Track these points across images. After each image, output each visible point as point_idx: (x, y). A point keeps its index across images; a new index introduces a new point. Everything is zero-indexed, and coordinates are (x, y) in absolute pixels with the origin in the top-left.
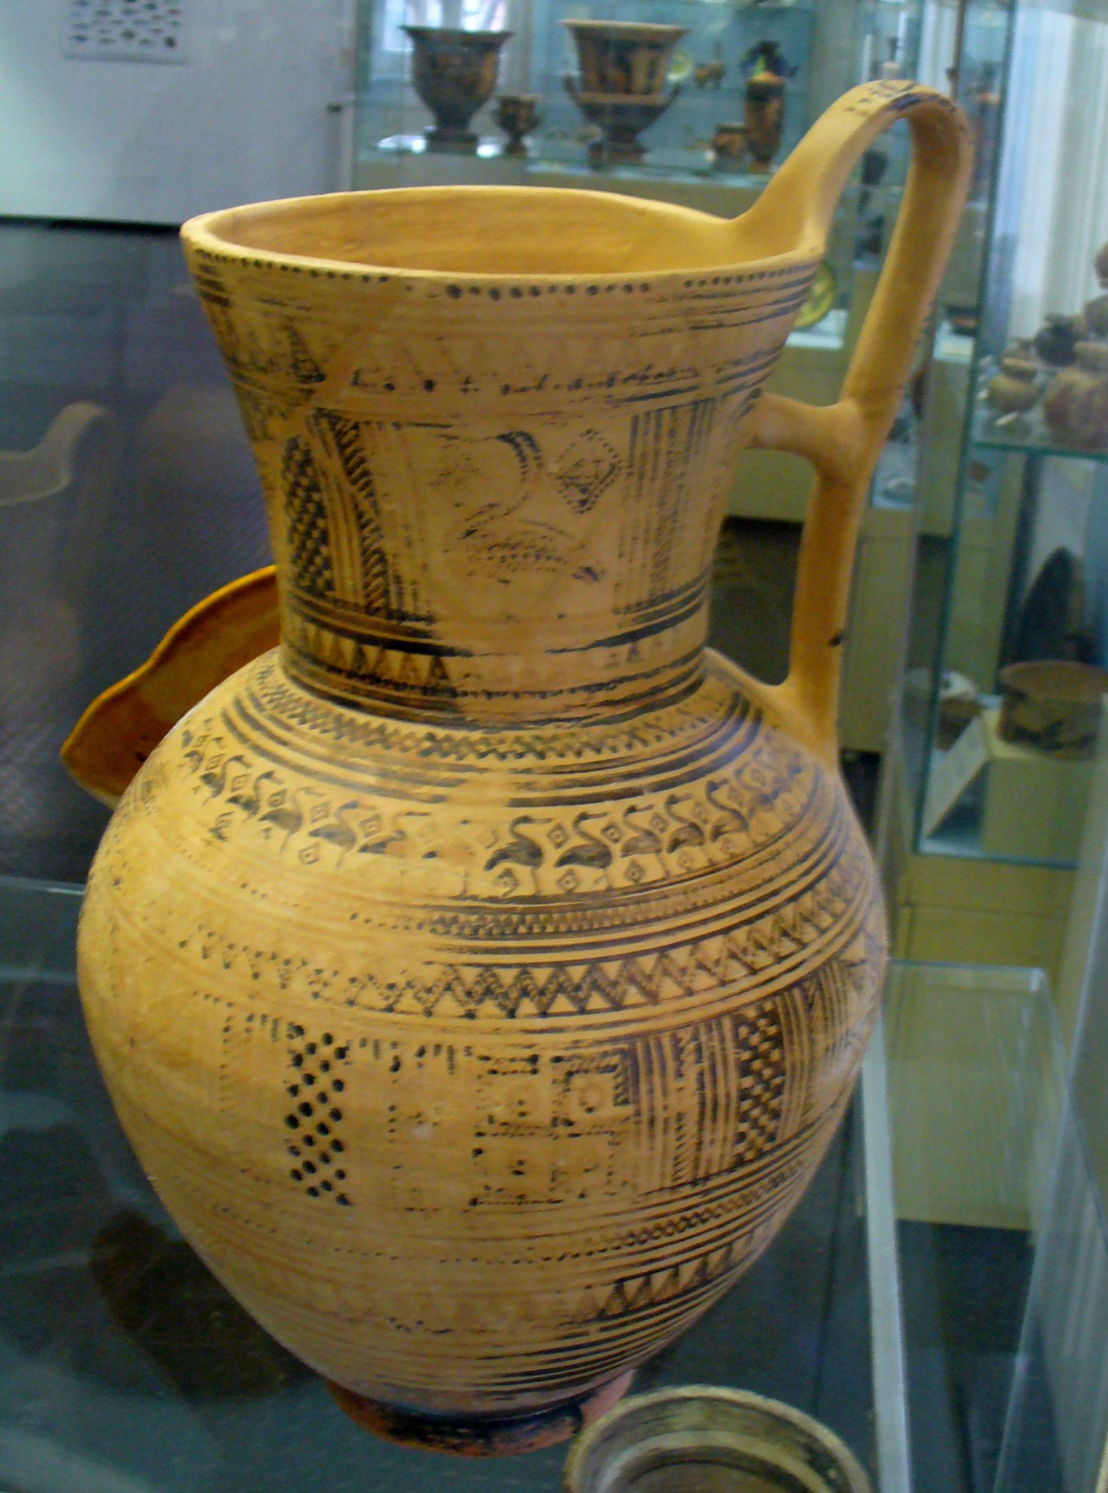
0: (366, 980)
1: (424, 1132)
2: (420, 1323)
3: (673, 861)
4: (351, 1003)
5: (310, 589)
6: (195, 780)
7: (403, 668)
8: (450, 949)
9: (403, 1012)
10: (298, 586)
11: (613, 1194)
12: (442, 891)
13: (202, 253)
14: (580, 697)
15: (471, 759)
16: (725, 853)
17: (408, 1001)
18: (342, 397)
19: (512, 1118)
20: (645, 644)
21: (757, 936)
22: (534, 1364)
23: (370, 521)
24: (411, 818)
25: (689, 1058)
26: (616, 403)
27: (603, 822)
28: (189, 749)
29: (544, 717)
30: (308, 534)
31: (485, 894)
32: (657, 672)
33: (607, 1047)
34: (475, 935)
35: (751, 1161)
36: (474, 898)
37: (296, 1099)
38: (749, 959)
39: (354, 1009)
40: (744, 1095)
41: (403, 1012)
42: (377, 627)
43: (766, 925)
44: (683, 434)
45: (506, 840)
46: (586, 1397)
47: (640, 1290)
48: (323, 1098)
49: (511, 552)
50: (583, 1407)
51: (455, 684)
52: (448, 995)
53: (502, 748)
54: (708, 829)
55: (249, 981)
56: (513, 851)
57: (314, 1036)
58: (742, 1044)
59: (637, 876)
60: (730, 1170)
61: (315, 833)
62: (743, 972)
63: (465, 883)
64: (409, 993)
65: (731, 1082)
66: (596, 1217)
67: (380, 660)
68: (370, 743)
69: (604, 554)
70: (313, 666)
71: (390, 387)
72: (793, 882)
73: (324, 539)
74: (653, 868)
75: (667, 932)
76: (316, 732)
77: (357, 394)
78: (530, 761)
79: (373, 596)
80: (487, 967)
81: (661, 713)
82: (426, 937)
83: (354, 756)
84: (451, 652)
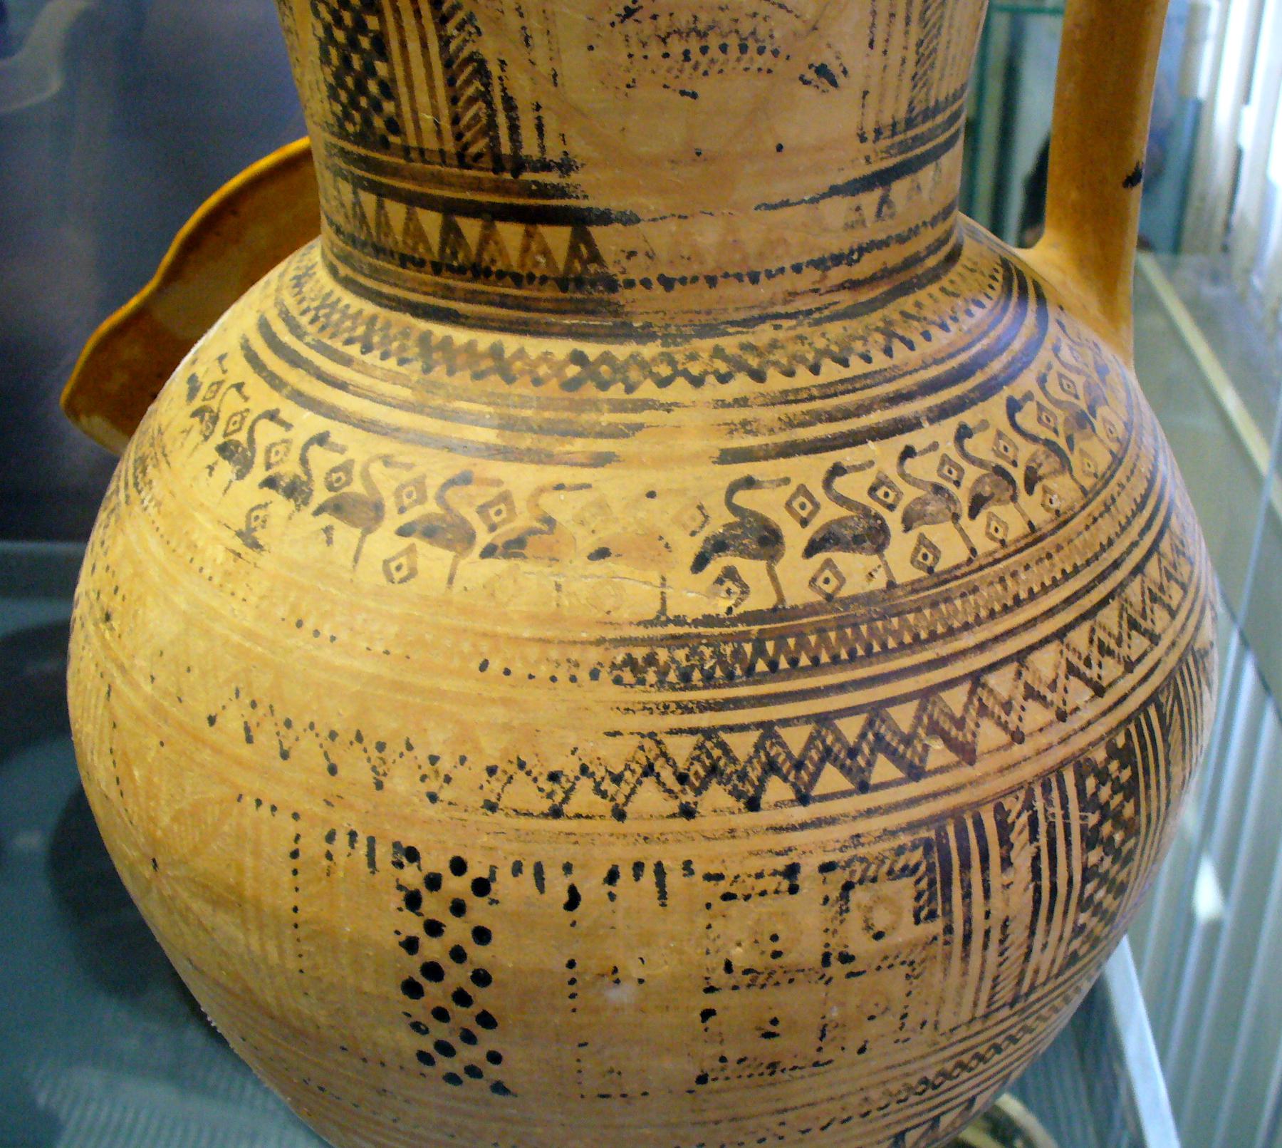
0: (512, 769)
1: (623, 995)
3: (976, 529)
4: (492, 807)
5: (360, 139)
6: (208, 453)
7: (526, 249)
9: (578, 816)
10: (344, 135)
11: (906, 1040)
12: (625, 614)
14: (810, 277)
15: (648, 390)
16: (1048, 510)
19: (758, 962)
20: (899, 189)
21: (1100, 634)
24: (562, 495)
27: (868, 478)
28: (198, 403)
29: (756, 313)
30: (353, 44)
31: (693, 613)
32: (914, 232)
33: (904, 839)
36: (679, 621)
37: (415, 957)
39: (499, 816)
40: (1088, 873)
41: (578, 816)
42: (478, 186)
43: (1109, 616)
45: (721, 519)
48: (458, 954)
51: (612, 270)
52: (649, 782)
53: (695, 369)
54: (1018, 475)
55: (324, 779)
56: (736, 537)
57: (435, 861)
58: (1087, 803)
59: (929, 562)
61: (403, 532)
62: (1089, 693)
64: (586, 784)
66: (879, 1071)
67: (484, 241)
68: (478, 376)
70: (377, 261)
72: (1134, 545)
75: (981, 647)
76: (392, 363)
78: (741, 385)
79: (468, 136)
80: (709, 733)
81: (921, 295)
82: (607, 690)
84: (605, 218)
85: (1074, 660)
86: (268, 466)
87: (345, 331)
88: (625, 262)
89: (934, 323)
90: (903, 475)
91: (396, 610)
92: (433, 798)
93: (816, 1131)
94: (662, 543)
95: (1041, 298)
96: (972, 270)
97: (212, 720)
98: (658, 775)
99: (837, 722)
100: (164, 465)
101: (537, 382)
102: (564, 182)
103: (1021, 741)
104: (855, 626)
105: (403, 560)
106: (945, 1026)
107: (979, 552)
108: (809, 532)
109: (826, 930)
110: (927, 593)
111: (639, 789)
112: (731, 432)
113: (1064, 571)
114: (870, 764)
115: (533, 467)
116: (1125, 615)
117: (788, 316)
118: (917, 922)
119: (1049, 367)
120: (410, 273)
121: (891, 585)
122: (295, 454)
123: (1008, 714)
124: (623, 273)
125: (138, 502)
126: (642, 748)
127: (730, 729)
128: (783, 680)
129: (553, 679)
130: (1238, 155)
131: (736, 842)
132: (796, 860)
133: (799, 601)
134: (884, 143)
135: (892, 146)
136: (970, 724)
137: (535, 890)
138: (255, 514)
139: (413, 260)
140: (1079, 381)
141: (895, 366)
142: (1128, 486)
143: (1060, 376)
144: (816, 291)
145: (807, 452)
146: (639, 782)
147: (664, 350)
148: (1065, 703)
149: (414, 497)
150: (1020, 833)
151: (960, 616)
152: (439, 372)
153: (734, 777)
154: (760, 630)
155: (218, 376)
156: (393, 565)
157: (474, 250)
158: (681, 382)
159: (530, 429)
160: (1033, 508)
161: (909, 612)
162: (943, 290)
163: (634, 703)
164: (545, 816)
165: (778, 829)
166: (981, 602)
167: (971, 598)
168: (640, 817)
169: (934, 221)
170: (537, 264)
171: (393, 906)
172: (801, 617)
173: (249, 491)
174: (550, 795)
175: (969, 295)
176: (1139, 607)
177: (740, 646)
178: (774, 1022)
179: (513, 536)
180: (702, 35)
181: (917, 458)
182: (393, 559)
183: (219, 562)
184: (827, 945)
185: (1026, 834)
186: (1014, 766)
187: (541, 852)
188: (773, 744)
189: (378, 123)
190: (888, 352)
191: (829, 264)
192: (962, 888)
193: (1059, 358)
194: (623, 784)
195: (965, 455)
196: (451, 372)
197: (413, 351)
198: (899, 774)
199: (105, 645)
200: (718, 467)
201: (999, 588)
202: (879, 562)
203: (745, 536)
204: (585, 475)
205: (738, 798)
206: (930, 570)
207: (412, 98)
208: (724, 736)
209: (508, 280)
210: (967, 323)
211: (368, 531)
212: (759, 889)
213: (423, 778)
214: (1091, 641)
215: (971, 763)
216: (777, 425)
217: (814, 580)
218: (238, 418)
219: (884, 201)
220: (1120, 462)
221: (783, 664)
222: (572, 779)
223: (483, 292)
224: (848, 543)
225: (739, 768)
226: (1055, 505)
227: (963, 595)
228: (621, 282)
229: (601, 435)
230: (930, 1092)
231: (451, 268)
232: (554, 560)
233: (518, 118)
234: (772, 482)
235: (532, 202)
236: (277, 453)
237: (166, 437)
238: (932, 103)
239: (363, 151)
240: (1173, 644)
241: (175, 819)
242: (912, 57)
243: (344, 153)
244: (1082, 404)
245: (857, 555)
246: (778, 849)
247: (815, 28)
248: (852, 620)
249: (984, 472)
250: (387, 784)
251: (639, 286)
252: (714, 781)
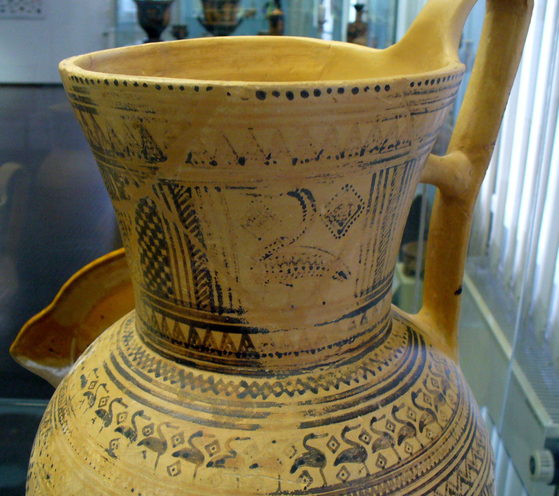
3: (401, 449)
7: (223, 342)
10: (149, 290)
13: (75, 78)
15: (272, 398)
16: (428, 438)
18: (178, 171)
20: (369, 312)
21: (450, 486)
23: (198, 251)
24: (239, 442)
26: (363, 166)
27: (358, 432)
28: (86, 390)
29: (314, 364)
32: (374, 327)
42: (205, 317)
43: (453, 479)
44: (398, 184)
45: (301, 452)
49: (293, 267)
51: (258, 350)
53: (290, 389)
54: (416, 425)
56: (307, 459)
61: (175, 455)
68: (204, 391)
69: (351, 263)
71: (214, 163)
72: (462, 447)
73: (167, 261)
74: (391, 457)
76: (168, 383)
77: (189, 169)
78: (308, 395)
79: (201, 298)
81: (377, 350)
83: (196, 399)
84: (255, 331)
86: (118, 423)
87: (148, 366)
88: (263, 348)
89: (382, 363)
90: (372, 429)
91: (173, 487)
94: (279, 461)
95: (423, 343)
96: (396, 336)
100: (72, 415)
101: (228, 394)
102: (239, 317)
105: (175, 467)
107: (402, 459)
108: (336, 456)
110: (382, 477)
112: (305, 415)
113: (435, 463)
116: (459, 477)
117: (326, 365)
119: (427, 376)
120: (175, 346)
121: (368, 475)
122: (129, 418)
124: (262, 351)
125: (61, 429)
130: (491, 215)
133: (332, 484)
134: (364, 297)
135: (367, 298)
138: (113, 443)
139: (177, 341)
140: (439, 380)
141: (368, 383)
142: (459, 423)
143: (432, 379)
144: (337, 354)
145: (334, 422)
147: (278, 381)
149: (179, 441)
151: (395, 486)
152: (188, 388)
155: (94, 379)
156: (171, 469)
157: (202, 340)
158: (284, 394)
160: (423, 438)
162: (386, 347)
166: (403, 479)
167: (399, 478)
169: (382, 321)
170: (228, 347)
172: (333, 490)
173: (110, 432)
175: (395, 348)
176: (464, 472)
179: (219, 459)
180: (295, 264)
181: (377, 422)
182: (171, 466)
183: (98, 461)
189: (165, 289)
190: (365, 377)
191: (342, 344)
193: (431, 371)
195: (396, 419)
196: (193, 388)
197: (177, 378)
199: (47, 489)
200: (300, 430)
201: (410, 472)
203: (311, 458)
204: (247, 434)
206: (383, 468)
207: (179, 282)
209: (216, 352)
210: (395, 361)
211: (160, 454)
214: (446, 490)
216: (323, 411)
217: (338, 475)
218: (104, 400)
219: (363, 318)
220: (456, 413)
223: (205, 357)
224: (351, 459)
226: (431, 436)
227: (396, 477)
228: (261, 355)
229: (254, 417)
231: (192, 346)
232: (236, 468)
233: (221, 293)
234: (321, 435)
235: (226, 324)
236: (122, 417)
237: (72, 402)
238: (382, 278)
239: (157, 298)
240: (478, 485)
242: (375, 264)
243: (148, 296)
244: (441, 390)
245: (355, 463)
247: (339, 259)
249: (403, 425)
251: (268, 357)
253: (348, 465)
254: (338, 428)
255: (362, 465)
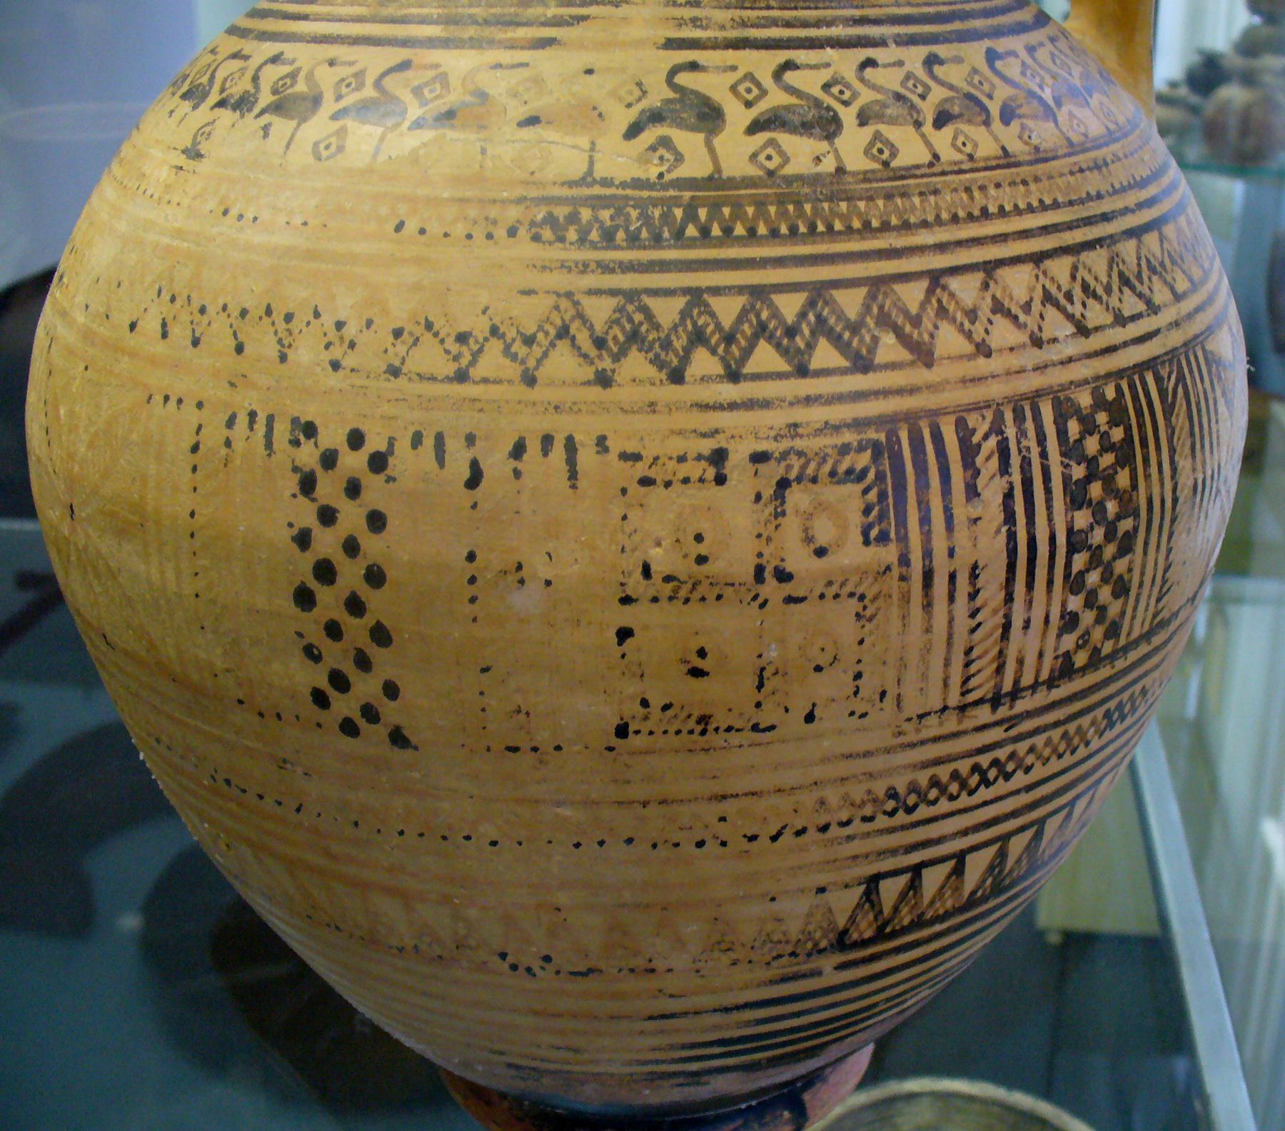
0: (419, 330)
1: (527, 600)
2: (547, 959)
3: (942, 140)
4: (394, 372)
8: (563, 266)
9: (485, 381)
12: (550, 173)
17: (492, 362)
19: (684, 568)
22: (733, 1026)
24: (499, 73)
25: (988, 465)
27: (825, 76)
33: (849, 437)
34: (608, 237)
35: (1083, 670)
36: (606, 182)
38: (1077, 309)
39: (401, 382)
41: (485, 381)
43: (1097, 261)
45: (659, 94)
46: (811, 1080)
47: (903, 896)
48: (351, 547)
50: (807, 1097)
52: (563, 345)
54: (994, 108)
56: (671, 111)
58: (1071, 451)
60: (1051, 683)
62: (1070, 329)
63: (591, 163)
64: (495, 346)
65: (1055, 518)
75: (941, 247)
80: (631, 295)
82: (525, 248)
85: (1053, 290)
92: (335, 365)
93: (764, 841)
94: (597, 112)
97: (133, 326)
98: (573, 339)
99: (773, 296)
103: (988, 354)
104: (798, 204)
106: (912, 709)
108: (753, 113)
109: (759, 536)
110: (881, 185)
111: (552, 353)
112: (680, 25)
114: (810, 346)
115: (473, 52)
118: (867, 542)
121: (840, 170)
123: (973, 323)
126: (557, 308)
127: (655, 293)
128: (715, 246)
129: (469, 237)
131: (655, 417)
132: (724, 445)
136: (927, 324)
137: (436, 465)
146: (553, 345)
148: (1040, 329)
150: (988, 459)
151: (918, 213)
153: (657, 345)
154: (693, 198)
159: (476, 22)
161: (860, 199)
163: (551, 261)
164: (449, 379)
165: (705, 407)
166: (942, 204)
167: (932, 198)
168: (551, 384)
171: (288, 493)
172: (737, 188)
174: (456, 358)
177: (670, 209)
178: (702, 653)
181: (879, 69)
184: (760, 555)
185: (994, 463)
186: (980, 379)
187: (442, 420)
188: (700, 314)
192: (920, 510)
194: (534, 346)
198: (844, 363)
200: (662, 53)
201: (964, 196)
202: (828, 148)
204: (524, 56)
205: (661, 368)
206: (886, 164)
208: (648, 300)
212: (681, 476)
213: (327, 346)
215: (929, 365)
217: (754, 156)
221: (716, 231)
222: (481, 340)
225: (662, 335)
227: (921, 194)
230: (901, 818)
232: (482, 127)
234: (718, 68)
241: (91, 445)
245: (804, 138)
246: (704, 429)
248: (796, 198)
250: (291, 355)
252: (634, 348)
253: (784, 138)
254: (770, 60)
255: (824, 146)
